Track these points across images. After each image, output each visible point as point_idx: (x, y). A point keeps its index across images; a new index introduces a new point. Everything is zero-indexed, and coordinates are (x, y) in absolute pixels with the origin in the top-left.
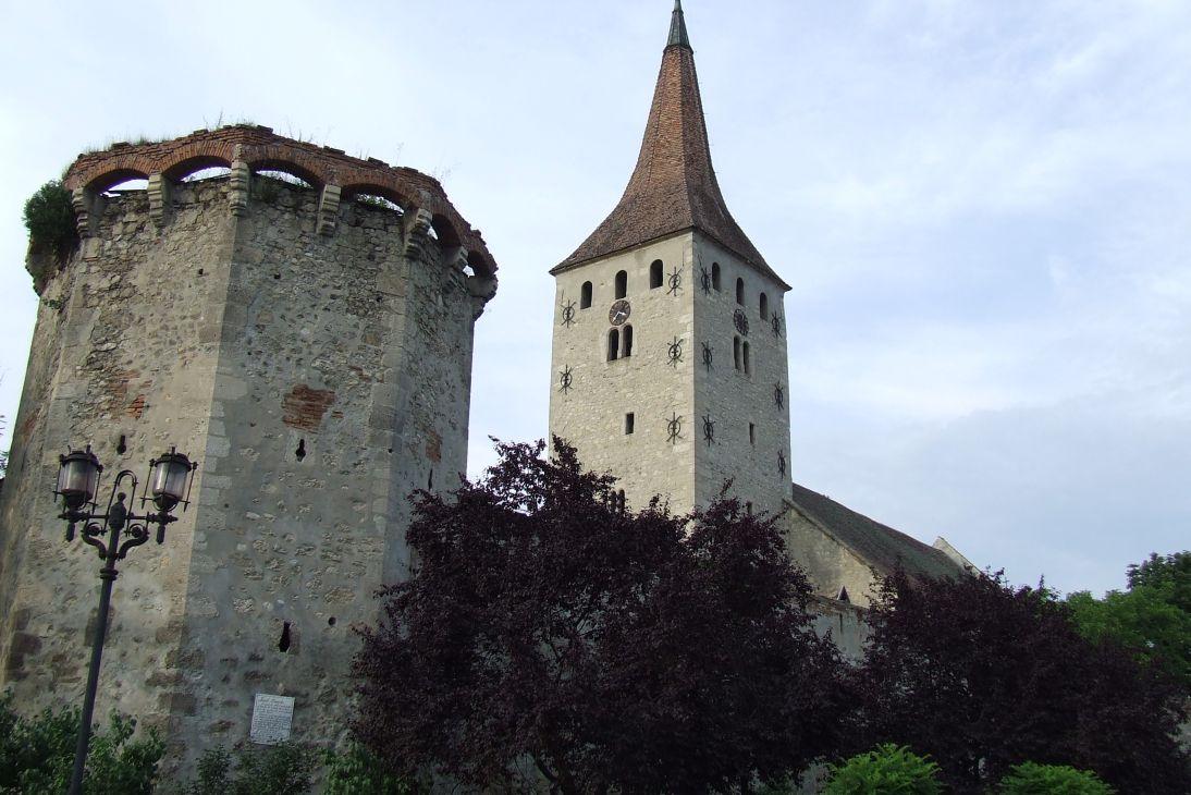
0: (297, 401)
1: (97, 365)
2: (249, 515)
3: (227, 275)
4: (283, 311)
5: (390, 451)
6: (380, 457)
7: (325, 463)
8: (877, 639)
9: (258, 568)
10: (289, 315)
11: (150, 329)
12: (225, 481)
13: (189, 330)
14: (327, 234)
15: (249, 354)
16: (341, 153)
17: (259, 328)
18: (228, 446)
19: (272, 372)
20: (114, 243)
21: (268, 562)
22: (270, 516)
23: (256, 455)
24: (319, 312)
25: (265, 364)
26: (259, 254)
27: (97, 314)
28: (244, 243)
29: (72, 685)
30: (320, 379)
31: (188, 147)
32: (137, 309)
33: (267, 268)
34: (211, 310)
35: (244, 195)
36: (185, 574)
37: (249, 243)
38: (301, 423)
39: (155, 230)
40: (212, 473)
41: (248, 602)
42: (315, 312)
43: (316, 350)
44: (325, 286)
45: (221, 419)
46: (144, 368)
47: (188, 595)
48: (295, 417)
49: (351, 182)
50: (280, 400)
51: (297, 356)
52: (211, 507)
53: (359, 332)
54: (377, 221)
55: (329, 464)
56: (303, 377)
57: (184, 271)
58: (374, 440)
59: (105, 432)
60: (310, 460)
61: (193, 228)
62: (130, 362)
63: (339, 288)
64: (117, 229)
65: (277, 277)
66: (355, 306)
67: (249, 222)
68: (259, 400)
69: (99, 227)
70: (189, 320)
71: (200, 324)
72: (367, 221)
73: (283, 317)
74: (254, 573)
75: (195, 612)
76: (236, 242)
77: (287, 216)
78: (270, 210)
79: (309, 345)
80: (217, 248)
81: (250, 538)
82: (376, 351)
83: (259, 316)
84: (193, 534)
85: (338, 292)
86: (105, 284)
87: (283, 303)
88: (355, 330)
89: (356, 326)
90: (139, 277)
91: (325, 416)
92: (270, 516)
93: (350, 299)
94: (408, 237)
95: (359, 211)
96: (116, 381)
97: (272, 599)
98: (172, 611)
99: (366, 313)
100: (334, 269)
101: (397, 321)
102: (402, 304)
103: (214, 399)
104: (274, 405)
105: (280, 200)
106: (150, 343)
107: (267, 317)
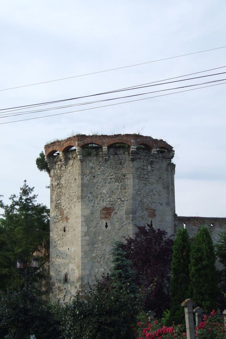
0: (104, 212)
1: (57, 207)
2: (95, 246)
3: (80, 180)
4: (97, 187)
5: (132, 221)
6: (129, 223)
7: (113, 228)
8: (50, 308)
9: (99, 260)
10: (99, 187)
11: (67, 196)
12: (87, 238)
13: (74, 196)
14: (106, 160)
15: (89, 201)
16: (106, 136)
17: (91, 193)
18: (87, 228)
19: (96, 205)
20: (57, 171)
21: (101, 258)
22: (100, 245)
23: (94, 229)
24: (107, 184)
25: (94, 203)
26: (88, 172)
27: (55, 193)
28: (83, 170)
29: (62, 294)
30: (110, 204)
31: (67, 143)
32: (63, 191)
33: (91, 175)
34: (78, 190)
35: (81, 156)
36: (80, 264)
37: (85, 169)
38: (106, 218)
39: (64, 167)
40: (84, 236)
41: (97, 269)
42: (106, 185)
43: (108, 196)
44: (108, 176)
45: (84, 221)
46: (66, 208)
47: (82, 269)
48: (104, 216)
49: (110, 144)
50: (99, 212)
51: (102, 199)
52: (84, 246)
53: (119, 188)
54: (121, 152)
55: (115, 228)
56: (105, 204)
57: (72, 179)
58: (127, 218)
59: (61, 226)
60: (109, 228)
61: (72, 165)
62: (64, 206)
63: (112, 175)
64: (57, 167)
65: (94, 177)
66: (117, 180)
67: (84, 163)
68: (93, 214)
69: (53, 166)
70: (74, 193)
71: (77, 195)
72: (118, 153)
73: (97, 188)
74: (98, 261)
75: (84, 274)
76: (81, 170)
77: (94, 158)
78: (90, 157)
79: (105, 195)
80: (78, 172)
81: (95, 252)
82: (125, 192)
83: (90, 190)
84: (81, 253)
85: (112, 177)
86: (56, 184)
87: (97, 184)
88: (118, 187)
89: (118, 186)
90: (63, 182)
91: (112, 214)
92: (100, 245)
93: (116, 178)
94: (130, 155)
95: (115, 150)
96: (62, 212)
97: (103, 268)
98: (79, 274)
99: (121, 181)
100: (110, 170)
101: (130, 182)
102: (131, 175)
103: (82, 216)
104: (98, 214)
105: (92, 153)
106: (67, 200)
107: (93, 190)
